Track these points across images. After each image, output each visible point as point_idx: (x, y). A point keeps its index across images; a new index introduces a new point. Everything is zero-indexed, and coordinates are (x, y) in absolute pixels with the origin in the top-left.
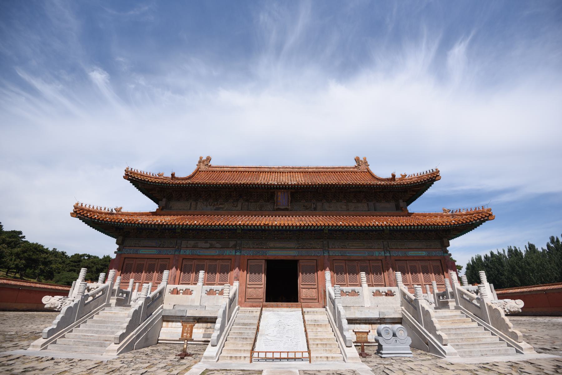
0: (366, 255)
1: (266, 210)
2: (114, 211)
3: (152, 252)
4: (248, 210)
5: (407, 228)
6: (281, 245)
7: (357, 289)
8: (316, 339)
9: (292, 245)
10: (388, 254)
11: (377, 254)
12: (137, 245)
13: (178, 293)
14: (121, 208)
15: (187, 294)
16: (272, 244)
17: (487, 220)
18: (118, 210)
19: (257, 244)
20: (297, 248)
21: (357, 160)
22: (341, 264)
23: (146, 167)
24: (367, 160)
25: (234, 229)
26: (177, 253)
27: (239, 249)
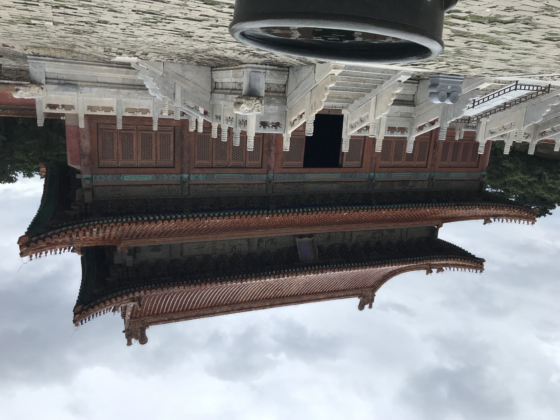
0: (216, 176)
1: (324, 234)
2: (492, 219)
3: (453, 175)
4: (344, 232)
5: (439, 204)
10: (372, 174)
11: (201, 177)
14: (485, 224)
15: (401, 128)
18: (487, 221)
20: (305, 182)
21: (143, 340)
22: (252, 162)
23: (452, 277)
24: (126, 341)
25: (195, 212)
26: (433, 174)
27: (184, 183)
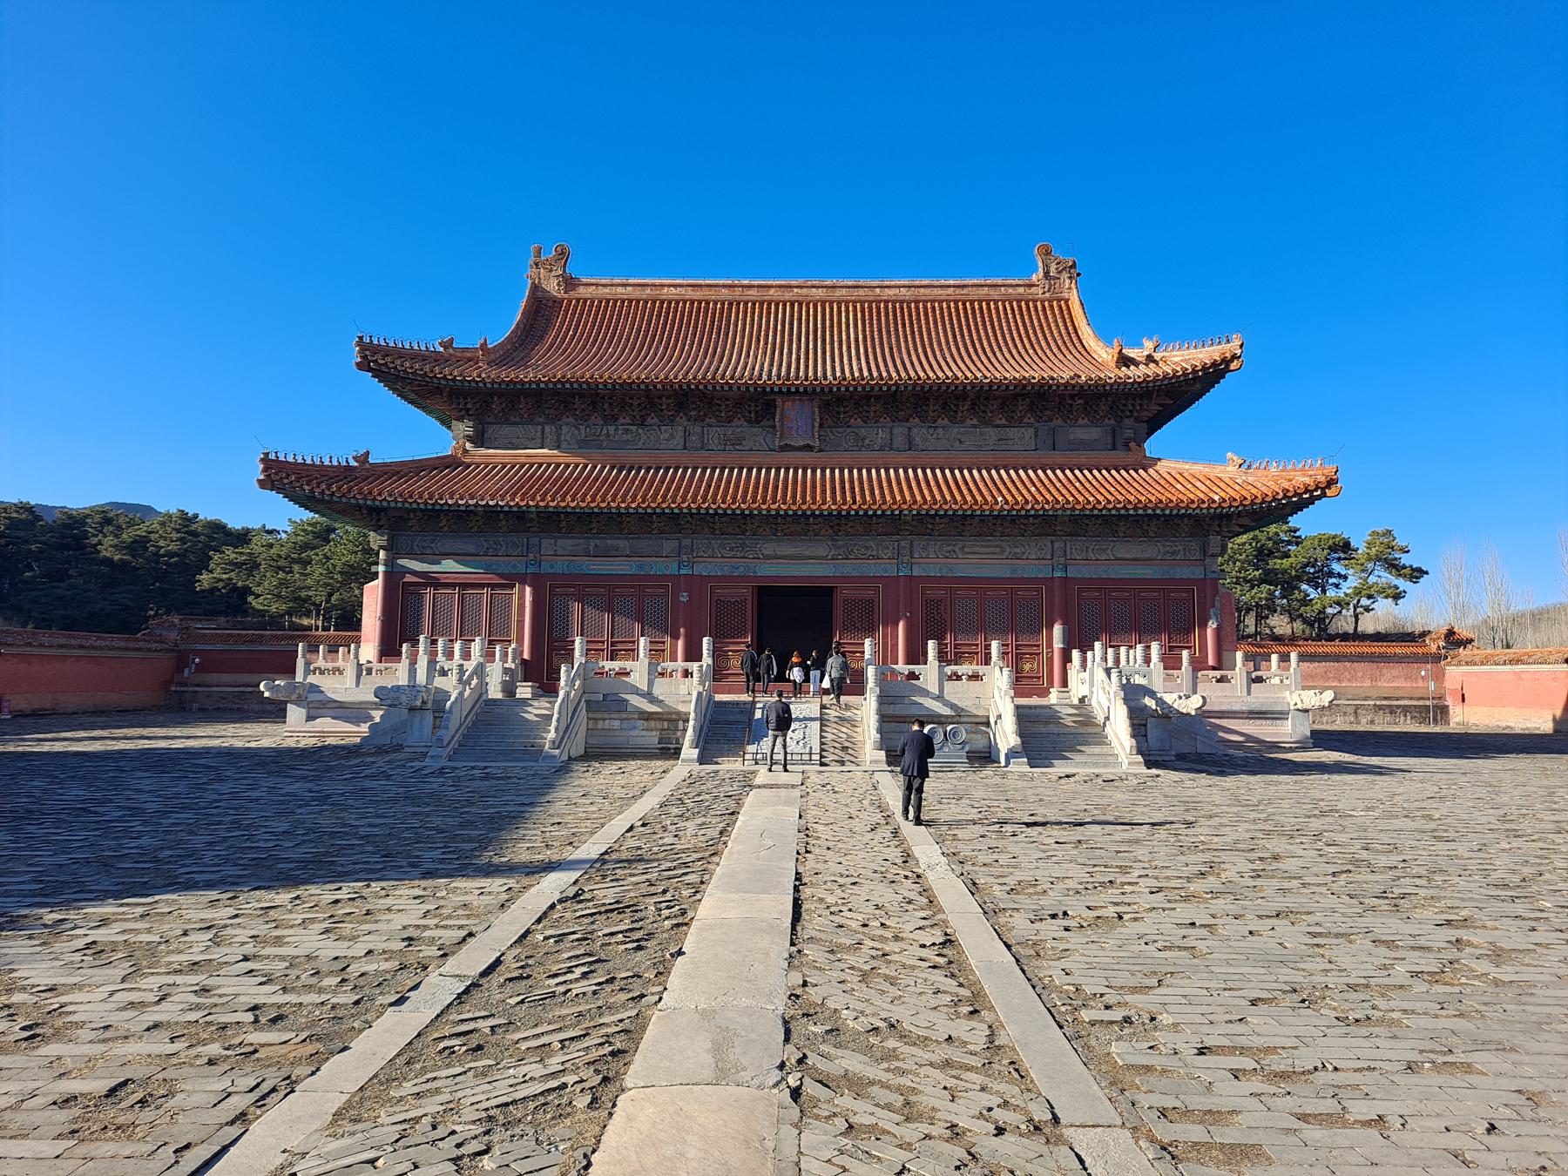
6: (791, 551)
7: (981, 669)
8: (263, 1097)
9: (821, 550)
12: (429, 551)
13: (959, 678)
16: (768, 548)
17: (1319, 498)
19: (732, 549)
